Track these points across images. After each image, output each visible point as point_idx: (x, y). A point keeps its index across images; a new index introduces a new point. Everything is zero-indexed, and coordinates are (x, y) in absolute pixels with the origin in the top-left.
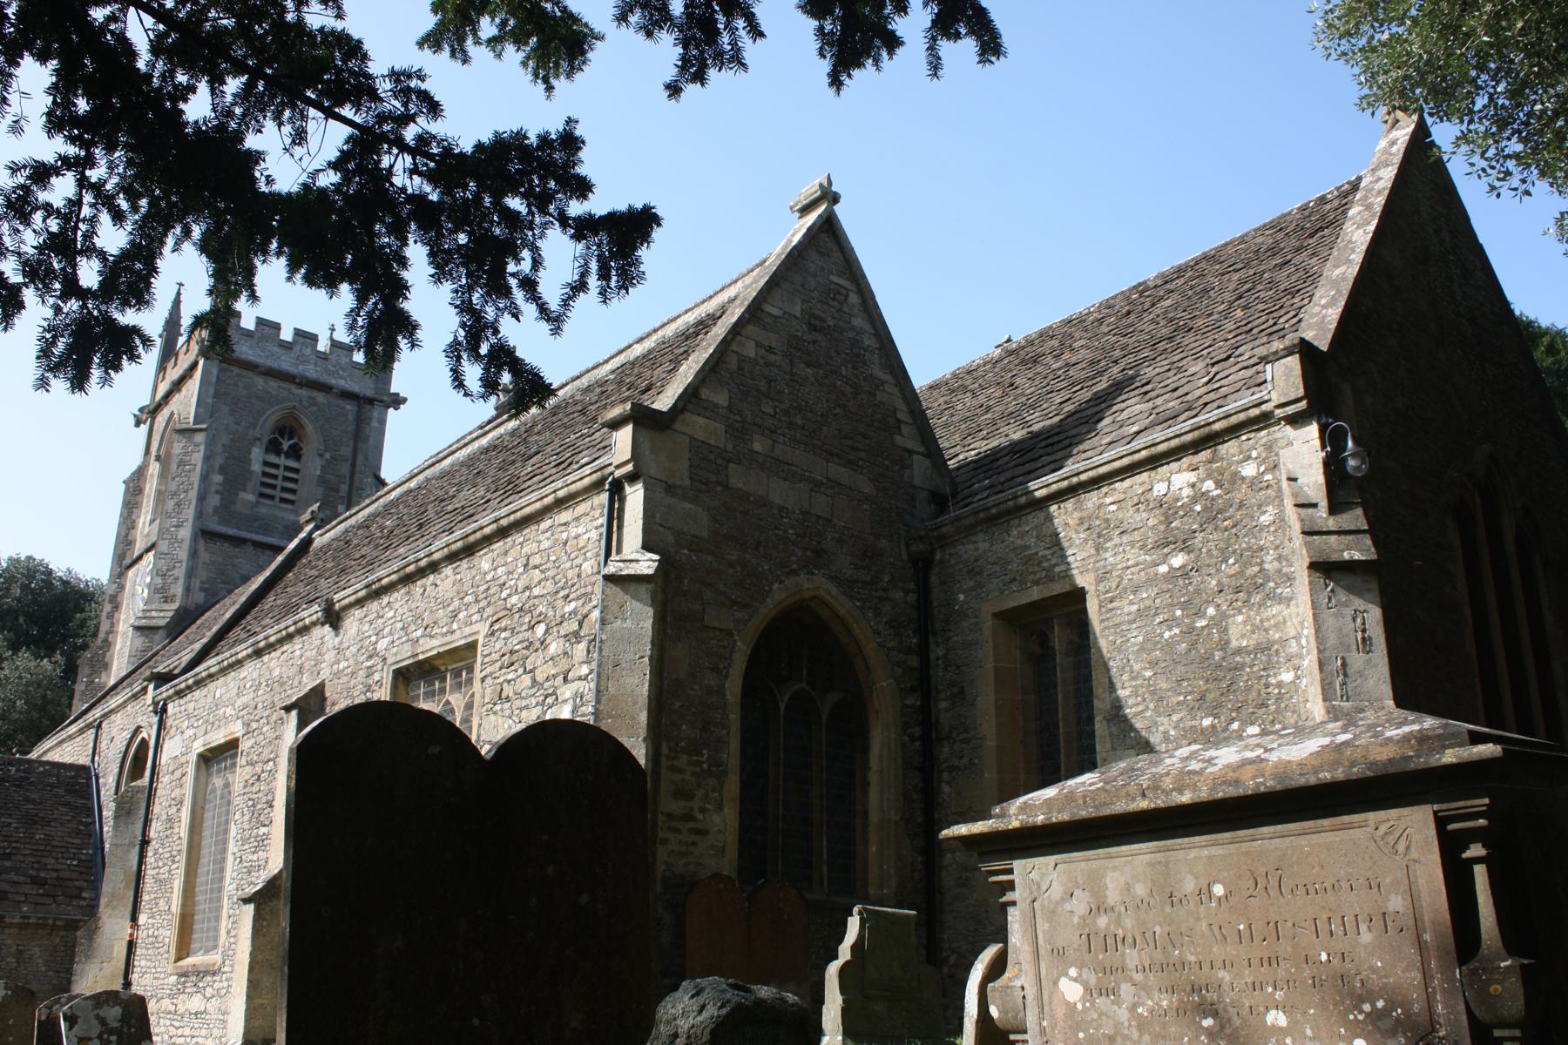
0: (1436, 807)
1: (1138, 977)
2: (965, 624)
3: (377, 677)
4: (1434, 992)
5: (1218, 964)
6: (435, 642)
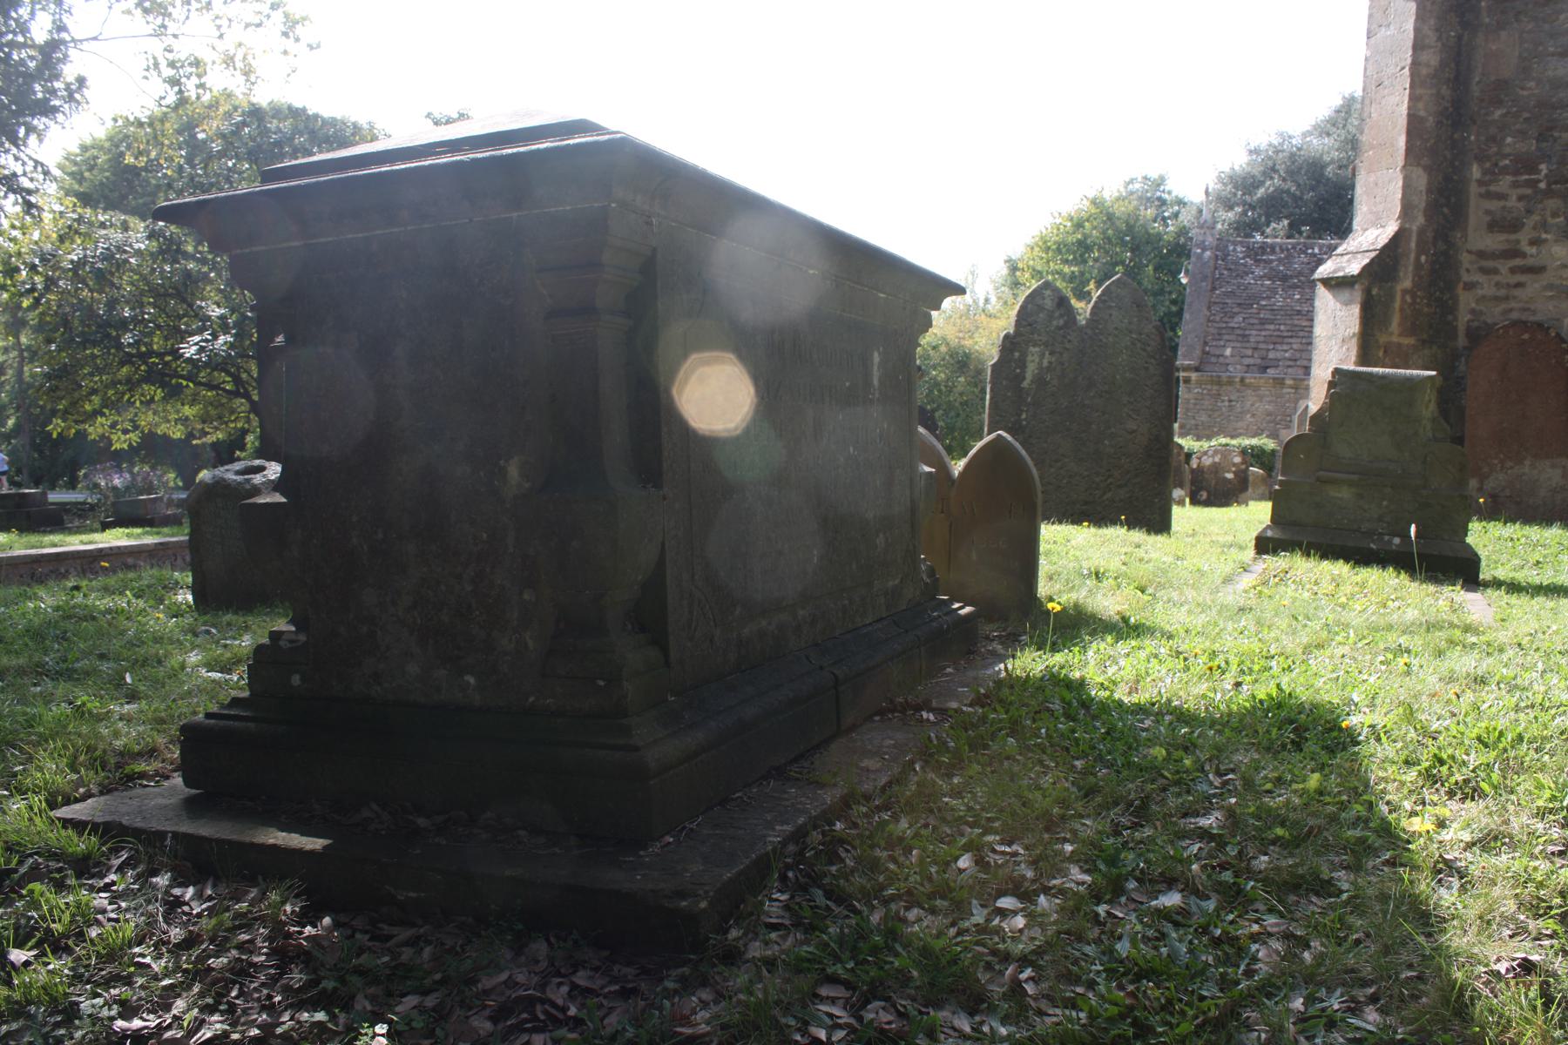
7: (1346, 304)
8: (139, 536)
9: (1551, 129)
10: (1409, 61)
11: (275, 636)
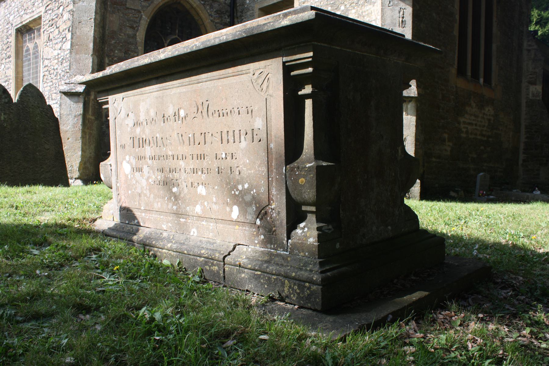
0: (285, 59)
1: (150, 162)
2: (248, 13)
3: (10, 32)
4: (272, 180)
5: (180, 157)
6: (28, 16)
7: (76, 102)
8: (47, 207)
9: (128, 51)
10: (94, 17)
11: (425, 196)
